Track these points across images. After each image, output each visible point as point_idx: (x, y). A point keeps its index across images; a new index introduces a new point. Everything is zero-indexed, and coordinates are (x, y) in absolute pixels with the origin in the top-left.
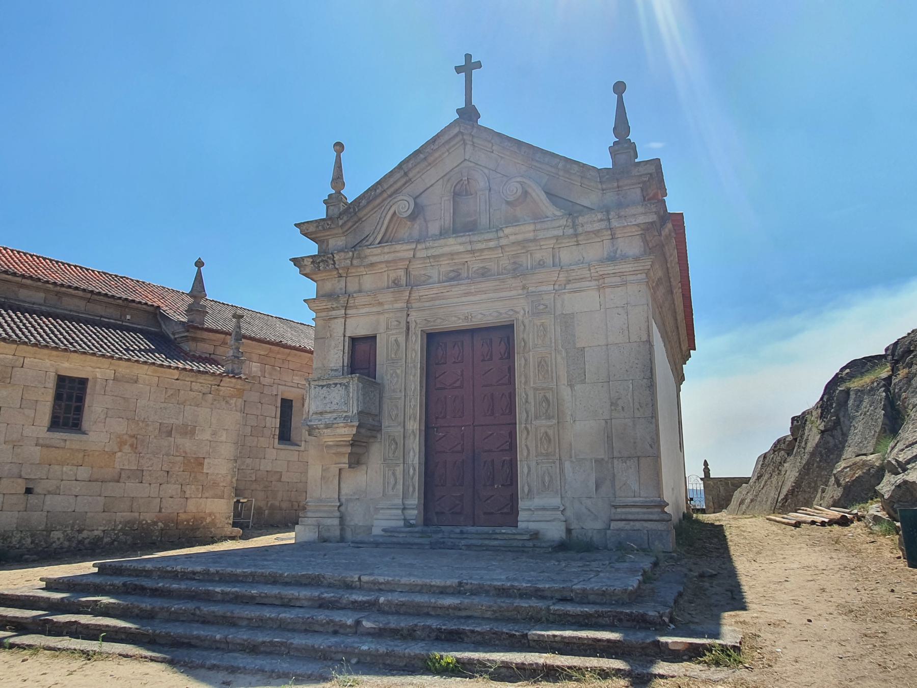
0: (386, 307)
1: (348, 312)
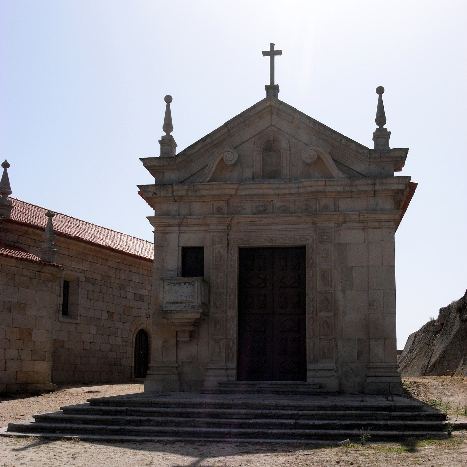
1: (182, 228)
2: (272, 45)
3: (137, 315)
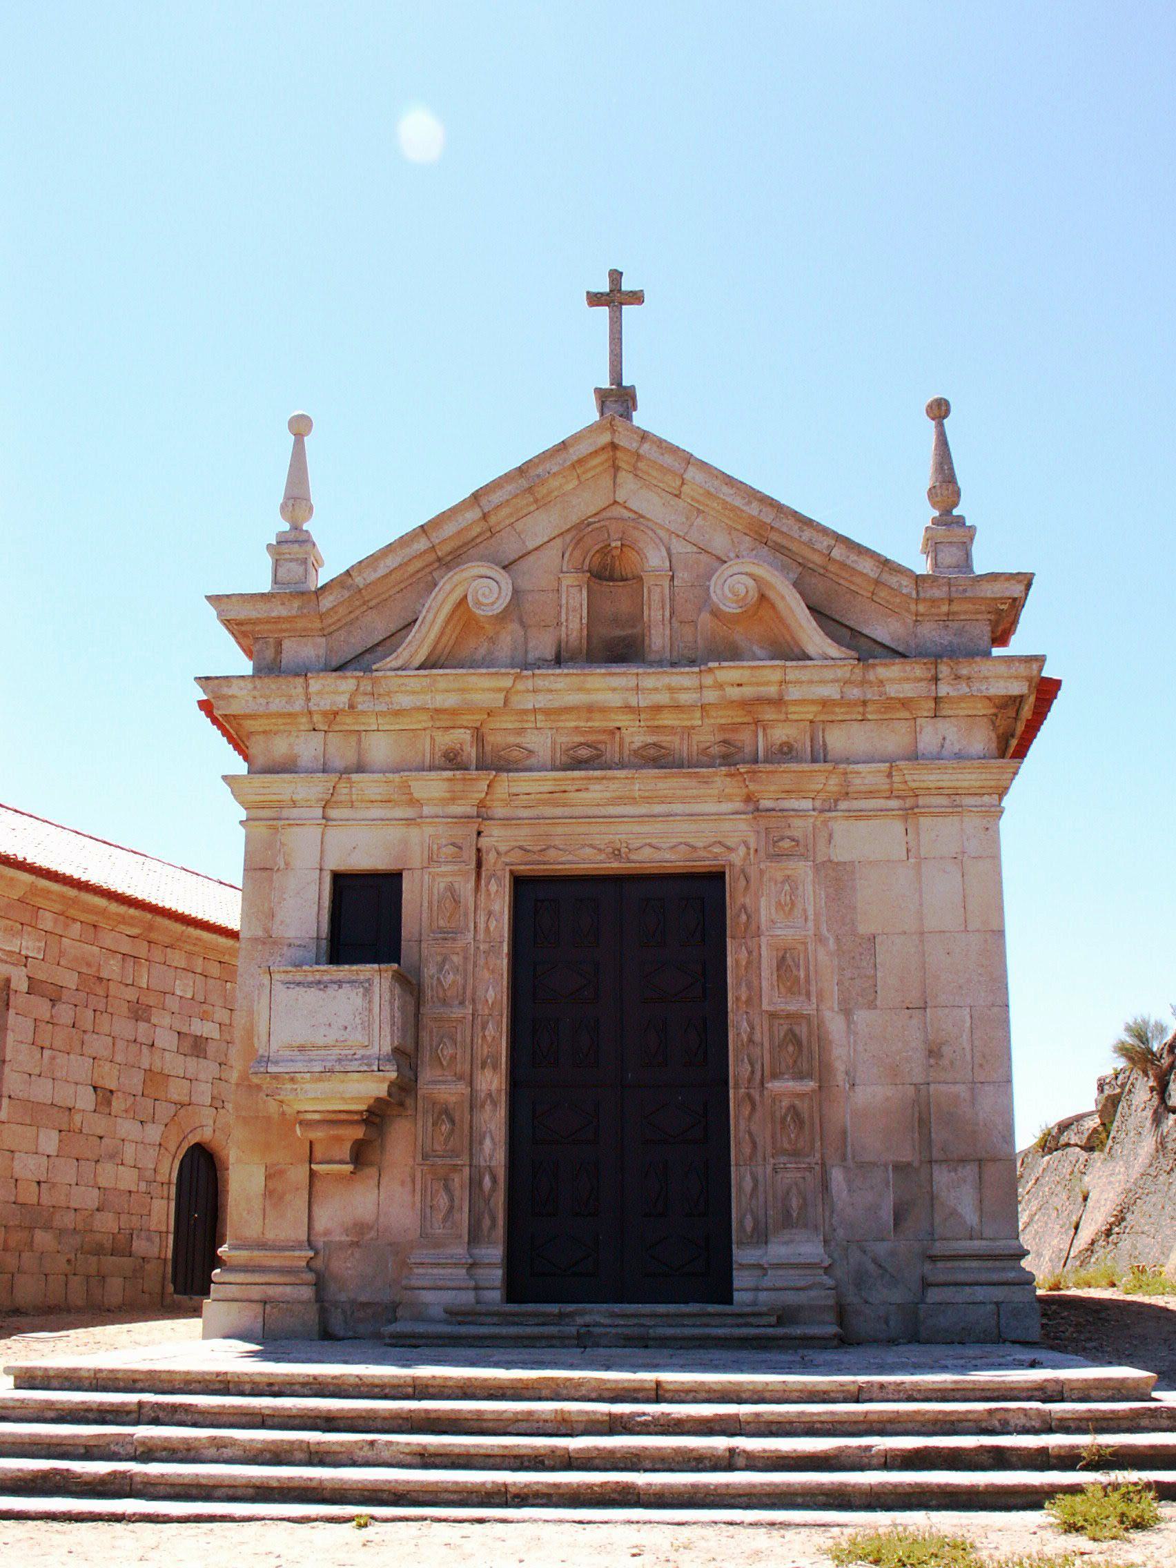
0: (426, 810)
1: (332, 813)
2: (616, 276)
3: (186, 1099)
